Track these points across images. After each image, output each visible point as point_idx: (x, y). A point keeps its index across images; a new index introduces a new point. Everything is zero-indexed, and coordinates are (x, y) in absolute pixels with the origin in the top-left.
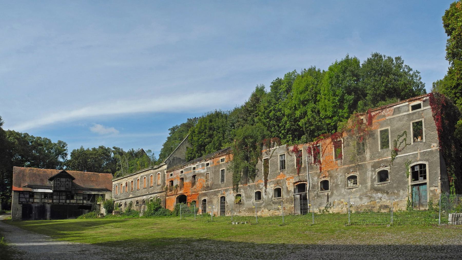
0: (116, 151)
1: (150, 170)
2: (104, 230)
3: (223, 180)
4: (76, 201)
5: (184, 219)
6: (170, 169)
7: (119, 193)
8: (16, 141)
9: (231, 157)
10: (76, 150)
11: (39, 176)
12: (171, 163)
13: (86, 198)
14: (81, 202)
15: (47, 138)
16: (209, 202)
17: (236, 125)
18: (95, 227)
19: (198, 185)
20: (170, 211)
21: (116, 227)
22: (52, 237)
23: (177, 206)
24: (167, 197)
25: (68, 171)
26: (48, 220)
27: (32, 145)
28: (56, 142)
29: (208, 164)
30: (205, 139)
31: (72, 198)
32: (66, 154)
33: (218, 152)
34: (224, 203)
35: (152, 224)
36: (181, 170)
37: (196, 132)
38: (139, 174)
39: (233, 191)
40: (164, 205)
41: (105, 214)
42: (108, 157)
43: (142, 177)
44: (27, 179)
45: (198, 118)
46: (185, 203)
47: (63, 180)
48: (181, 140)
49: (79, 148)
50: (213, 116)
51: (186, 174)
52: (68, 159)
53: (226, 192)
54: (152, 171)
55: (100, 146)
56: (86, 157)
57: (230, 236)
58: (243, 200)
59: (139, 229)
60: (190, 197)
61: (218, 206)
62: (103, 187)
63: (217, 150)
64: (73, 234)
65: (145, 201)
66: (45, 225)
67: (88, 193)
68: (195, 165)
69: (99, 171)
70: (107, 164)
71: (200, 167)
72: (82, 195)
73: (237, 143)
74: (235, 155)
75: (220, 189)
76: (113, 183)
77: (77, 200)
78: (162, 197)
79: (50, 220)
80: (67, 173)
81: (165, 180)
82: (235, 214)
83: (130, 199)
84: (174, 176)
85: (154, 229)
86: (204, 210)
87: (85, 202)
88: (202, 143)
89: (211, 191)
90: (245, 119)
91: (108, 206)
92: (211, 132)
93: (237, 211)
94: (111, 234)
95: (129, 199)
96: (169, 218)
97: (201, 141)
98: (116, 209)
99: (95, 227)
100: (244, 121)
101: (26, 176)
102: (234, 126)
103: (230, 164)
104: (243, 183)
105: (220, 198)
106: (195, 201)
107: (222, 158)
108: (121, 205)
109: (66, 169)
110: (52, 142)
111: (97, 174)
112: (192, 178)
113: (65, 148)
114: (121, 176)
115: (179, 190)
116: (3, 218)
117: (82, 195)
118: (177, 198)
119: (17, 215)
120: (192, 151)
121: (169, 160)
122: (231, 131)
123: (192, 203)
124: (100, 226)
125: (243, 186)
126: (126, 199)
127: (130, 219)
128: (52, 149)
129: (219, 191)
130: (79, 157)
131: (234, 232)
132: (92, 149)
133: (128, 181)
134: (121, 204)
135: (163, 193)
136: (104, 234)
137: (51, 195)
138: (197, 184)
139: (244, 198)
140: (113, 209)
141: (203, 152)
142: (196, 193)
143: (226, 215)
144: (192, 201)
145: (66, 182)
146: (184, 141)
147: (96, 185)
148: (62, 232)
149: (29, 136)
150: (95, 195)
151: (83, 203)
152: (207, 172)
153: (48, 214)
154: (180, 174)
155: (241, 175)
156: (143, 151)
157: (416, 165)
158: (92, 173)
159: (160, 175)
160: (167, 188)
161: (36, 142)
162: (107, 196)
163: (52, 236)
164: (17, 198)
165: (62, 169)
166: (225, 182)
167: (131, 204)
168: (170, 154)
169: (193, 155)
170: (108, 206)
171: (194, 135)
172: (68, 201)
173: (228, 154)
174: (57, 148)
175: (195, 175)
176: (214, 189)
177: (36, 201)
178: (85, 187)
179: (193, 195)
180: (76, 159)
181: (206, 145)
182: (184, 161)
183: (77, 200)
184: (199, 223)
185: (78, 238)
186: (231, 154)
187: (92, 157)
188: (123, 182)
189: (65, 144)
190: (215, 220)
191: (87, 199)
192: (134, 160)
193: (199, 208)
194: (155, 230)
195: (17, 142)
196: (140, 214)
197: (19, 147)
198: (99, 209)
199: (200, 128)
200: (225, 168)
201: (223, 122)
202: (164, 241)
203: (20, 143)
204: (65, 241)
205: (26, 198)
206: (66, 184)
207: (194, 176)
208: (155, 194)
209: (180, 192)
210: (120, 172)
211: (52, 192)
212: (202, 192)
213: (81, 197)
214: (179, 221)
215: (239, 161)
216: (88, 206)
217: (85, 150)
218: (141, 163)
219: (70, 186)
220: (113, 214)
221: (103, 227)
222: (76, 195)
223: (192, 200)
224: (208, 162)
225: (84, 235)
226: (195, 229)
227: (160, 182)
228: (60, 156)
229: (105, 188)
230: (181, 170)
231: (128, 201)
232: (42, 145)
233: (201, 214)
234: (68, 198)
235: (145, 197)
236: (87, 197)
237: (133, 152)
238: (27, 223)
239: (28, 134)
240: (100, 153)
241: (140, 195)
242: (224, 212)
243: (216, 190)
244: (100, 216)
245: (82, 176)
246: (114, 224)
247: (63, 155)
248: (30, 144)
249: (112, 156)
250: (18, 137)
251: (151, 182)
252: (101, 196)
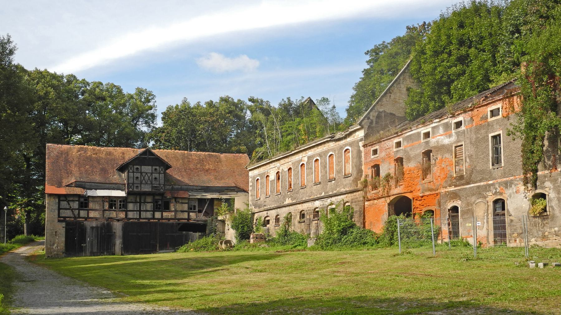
0: (256, 106)
1: (327, 142)
2: (229, 277)
3: (497, 160)
4: (175, 215)
5: (407, 253)
6: (372, 139)
7: (263, 195)
8: (51, 92)
9: (515, 104)
10: (172, 107)
11: (98, 161)
12: (374, 125)
13: (195, 206)
14: (185, 215)
15: (113, 84)
16: (464, 213)
17: (523, 29)
18: (210, 269)
19: (438, 174)
20: (375, 234)
21: (256, 271)
22: (114, 293)
23: (390, 222)
24: (366, 203)
25: (158, 150)
26: (118, 255)
27: (84, 99)
28: (133, 92)
29: (459, 124)
30: (450, 67)
31: (167, 208)
32: (153, 117)
33: (484, 96)
34: (504, 215)
35: (335, 264)
36: (397, 140)
37: (429, 53)
38: (304, 153)
39: (524, 185)
40: (362, 221)
41: (234, 241)
42: (240, 120)
43: (309, 158)
44: (75, 169)
45: (429, 25)
46: (408, 216)
47: (147, 169)
48: (394, 74)
49: (180, 103)
50: (466, 13)
51: (408, 149)
52: (157, 127)
53: (507, 188)
54: (332, 144)
55: (223, 96)
56: (193, 121)
57: (529, 299)
58: (552, 207)
59: (305, 276)
60: (418, 202)
61: (488, 222)
62: (230, 183)
63: (480, 92)
64: (162, 286)
65: (318, 212)
66: (109, 267)
67: (199, 197)
68: (428, 127)
69: (220, 149)
70: (237, 136)
71: (441, 131)
72: (187, 201)
73: (532, 69)
74: (525, 98)
75: (491, 182)
76: (251, 174)
77: (176, 211)
78: (355, 202)
79: (122, 255)
80: (153, 154)
81: (361, 164)
82: (533, 241)
83: (287, 208)
84: (381, 155)
85: (339, 274)
86: (454, 232)
87: (192, 215)
88: (442, 77)
89: (470, 188)
90: (544, 15)
91: (241, 223)
92: (463, 51)
93: (536, 234)
94: (242, 285)
95: (284, 209)
96: (374, 249)
97: (440, 72)
98: (257, 230)
99: (210, 269)
100: (541, 21)
101: (72, 163)
102: (519, 32)
103: (514, 120)
104: (550, 166)
105: (491, 204)
106: (433, 212)
107: (493, 107)
108: (268, 221)
109: (154, 147)
110: (125, 92)
111: (216, 156)
112: (423, 158)
113: (151, 104)
114: (266, 157)
115: (393, 186)
116: (29, 251)
117: (187, 201)
118: (389, 204)
119: (55, 245)
120: (421, 97)
121: (369, 118)
122: (512, 43)
123: (425, 214)
124: (221, 268)
125: (551, 173)
126: (277, 208)
127: (287, 251)
128: (124, 105)
129: (490, 185)
130: (179, 120)
131: (538, 286)
132: (206, 103)
133: (281, 168)
134: (267, 219)
135: (357, 193)
136: (228, 286)
137: (124, 201)
138: (435, 170)
139: (554, 203)
140: (251, 230)
141: (445, 98)
142: (434, 192)
143: (508, 244)
144: (426, 211)
145: (152, 173)
146: (401, 75)
147: (216, 179)
148: (139, 282)
149: (78, 80)
150: (212, 200)
151: (189, 219)
152: (458, 142)
153: (118, 243)
154: (395, 150)
155: (543, 146)
156: (311, 101)
158: (207, 153)
159: (349, 152)
160: (366, 181)
161: (92, 92)
162: (239, 203)
163: (116, 291)
164: (54, 210)
165: (145, 146)
166: (503, 165)
167: (289, 220)
168: (371, 104)
169: (422, 106)
170: (241, 223)
171: (422, 61)
172: (158, 215)
173: (507, 97)
174: (136, 106)
175: (430, 151)
176: (476, 183)
177: (92, 214)
178: (191, 184)
179: (427, 196)
180: (174, 124)
181: (453, 81)
182: (402, 119)
183: (176, 211)
184: (443, 262)
185: (169, 295)
186: (515, 97)
187: (206, 121)
188: (272, 170)
189: (150, 95)
190: (481, 256)
191: (197, 210)
192: (291, 122)
193: (443, 226)
194: (341, 278)
195: (52, 94)
196: (309, 241)
197: (57, 104)
198: (222, 231)
199: (437, 43)
200: (501, 132)
201: (491, 26)
202: (363, 305)
203: (59, 96)
204: (139, 302)
205: (72, 210)
206: (153, 177)
207: (427, 154)
208: (339, 197)
209: (397, 191)
210: (262, 149)
211: (124, 195)
212: (447, 190)
213: (184, 205)
214: (396, 257)
215: (537, 112)
216: (199, 224)
217: (192, 105)
218: (307, 127)
219: (162, 181)
220: (252, 241)
221: (228, 270)
222: (174, 200)
223: (425, 209)
224: (460, 118)
225: (184, 289)
226: (436, 277)
227: (350, 169)
228: (141, 120)
229: (233, 185)
230: (397, 140)
231: (283, 212)
232: (103, 99)
233: (447, 240)
234: (156, 208)
235: (317, 204)
236: (197, 205)
237: (290, 104)
238: (76, 262)
239: (75, 77)
240: (223, 112)
241: (307, 198)
242: (505, 235)
243: (482, 184)
244: (224, 246)
245: (186, 160)
246: (252, 262)
247: (147, 117)
248: (80, 96)
249: (247, 118)
250: (55, 82)
251: (331, 168)
252: (225, 202)
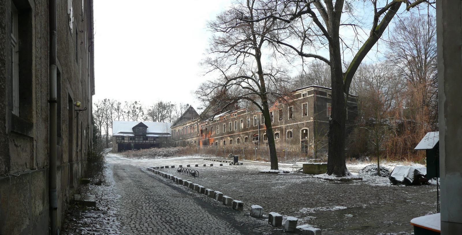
14: (153, 142)
47: (141, 128)
157: (304, 129)
172: (144, 142)
183: (150, 140)
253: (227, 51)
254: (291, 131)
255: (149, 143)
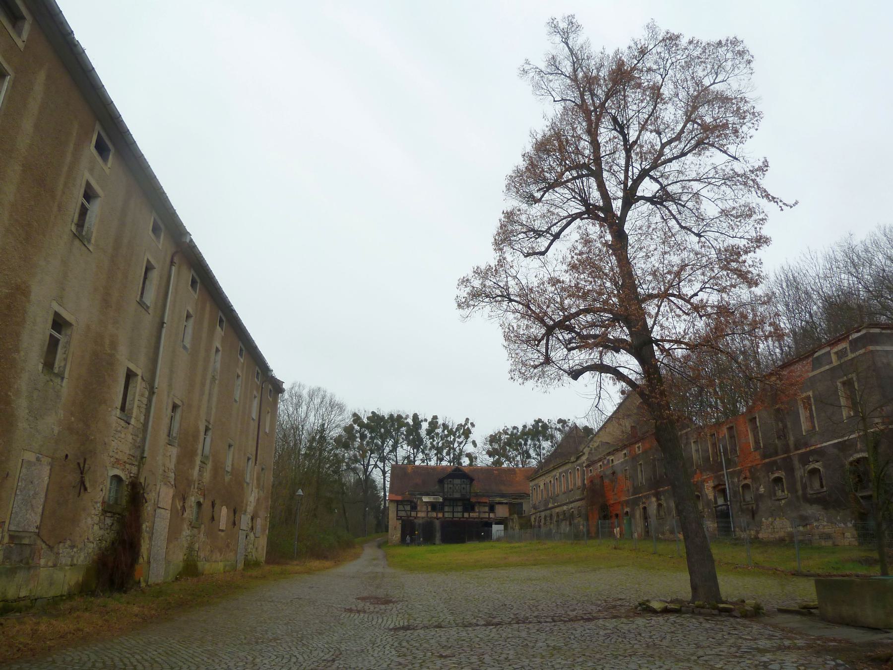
14: (486, 515)
172: (466, 515)
253: (543, 249)
254: (816, 467)
255: (479, 518)
